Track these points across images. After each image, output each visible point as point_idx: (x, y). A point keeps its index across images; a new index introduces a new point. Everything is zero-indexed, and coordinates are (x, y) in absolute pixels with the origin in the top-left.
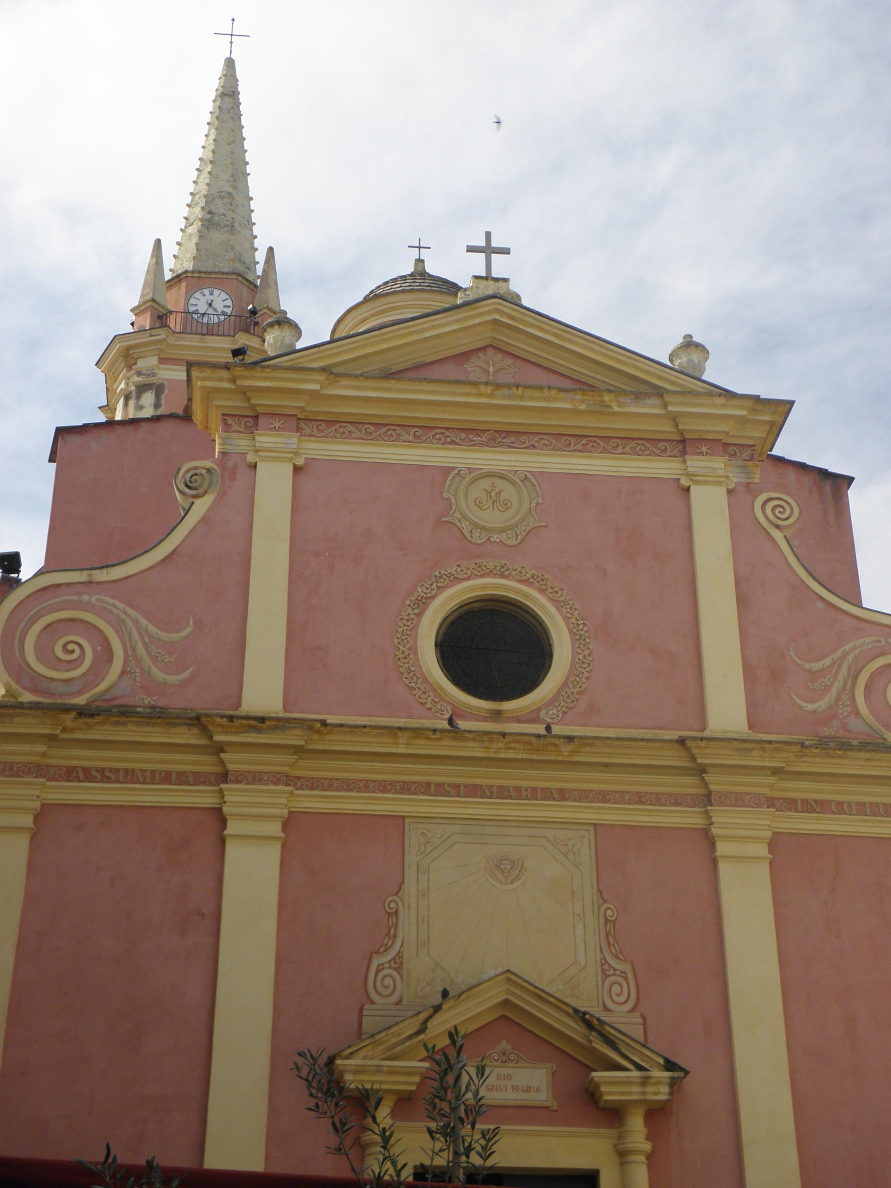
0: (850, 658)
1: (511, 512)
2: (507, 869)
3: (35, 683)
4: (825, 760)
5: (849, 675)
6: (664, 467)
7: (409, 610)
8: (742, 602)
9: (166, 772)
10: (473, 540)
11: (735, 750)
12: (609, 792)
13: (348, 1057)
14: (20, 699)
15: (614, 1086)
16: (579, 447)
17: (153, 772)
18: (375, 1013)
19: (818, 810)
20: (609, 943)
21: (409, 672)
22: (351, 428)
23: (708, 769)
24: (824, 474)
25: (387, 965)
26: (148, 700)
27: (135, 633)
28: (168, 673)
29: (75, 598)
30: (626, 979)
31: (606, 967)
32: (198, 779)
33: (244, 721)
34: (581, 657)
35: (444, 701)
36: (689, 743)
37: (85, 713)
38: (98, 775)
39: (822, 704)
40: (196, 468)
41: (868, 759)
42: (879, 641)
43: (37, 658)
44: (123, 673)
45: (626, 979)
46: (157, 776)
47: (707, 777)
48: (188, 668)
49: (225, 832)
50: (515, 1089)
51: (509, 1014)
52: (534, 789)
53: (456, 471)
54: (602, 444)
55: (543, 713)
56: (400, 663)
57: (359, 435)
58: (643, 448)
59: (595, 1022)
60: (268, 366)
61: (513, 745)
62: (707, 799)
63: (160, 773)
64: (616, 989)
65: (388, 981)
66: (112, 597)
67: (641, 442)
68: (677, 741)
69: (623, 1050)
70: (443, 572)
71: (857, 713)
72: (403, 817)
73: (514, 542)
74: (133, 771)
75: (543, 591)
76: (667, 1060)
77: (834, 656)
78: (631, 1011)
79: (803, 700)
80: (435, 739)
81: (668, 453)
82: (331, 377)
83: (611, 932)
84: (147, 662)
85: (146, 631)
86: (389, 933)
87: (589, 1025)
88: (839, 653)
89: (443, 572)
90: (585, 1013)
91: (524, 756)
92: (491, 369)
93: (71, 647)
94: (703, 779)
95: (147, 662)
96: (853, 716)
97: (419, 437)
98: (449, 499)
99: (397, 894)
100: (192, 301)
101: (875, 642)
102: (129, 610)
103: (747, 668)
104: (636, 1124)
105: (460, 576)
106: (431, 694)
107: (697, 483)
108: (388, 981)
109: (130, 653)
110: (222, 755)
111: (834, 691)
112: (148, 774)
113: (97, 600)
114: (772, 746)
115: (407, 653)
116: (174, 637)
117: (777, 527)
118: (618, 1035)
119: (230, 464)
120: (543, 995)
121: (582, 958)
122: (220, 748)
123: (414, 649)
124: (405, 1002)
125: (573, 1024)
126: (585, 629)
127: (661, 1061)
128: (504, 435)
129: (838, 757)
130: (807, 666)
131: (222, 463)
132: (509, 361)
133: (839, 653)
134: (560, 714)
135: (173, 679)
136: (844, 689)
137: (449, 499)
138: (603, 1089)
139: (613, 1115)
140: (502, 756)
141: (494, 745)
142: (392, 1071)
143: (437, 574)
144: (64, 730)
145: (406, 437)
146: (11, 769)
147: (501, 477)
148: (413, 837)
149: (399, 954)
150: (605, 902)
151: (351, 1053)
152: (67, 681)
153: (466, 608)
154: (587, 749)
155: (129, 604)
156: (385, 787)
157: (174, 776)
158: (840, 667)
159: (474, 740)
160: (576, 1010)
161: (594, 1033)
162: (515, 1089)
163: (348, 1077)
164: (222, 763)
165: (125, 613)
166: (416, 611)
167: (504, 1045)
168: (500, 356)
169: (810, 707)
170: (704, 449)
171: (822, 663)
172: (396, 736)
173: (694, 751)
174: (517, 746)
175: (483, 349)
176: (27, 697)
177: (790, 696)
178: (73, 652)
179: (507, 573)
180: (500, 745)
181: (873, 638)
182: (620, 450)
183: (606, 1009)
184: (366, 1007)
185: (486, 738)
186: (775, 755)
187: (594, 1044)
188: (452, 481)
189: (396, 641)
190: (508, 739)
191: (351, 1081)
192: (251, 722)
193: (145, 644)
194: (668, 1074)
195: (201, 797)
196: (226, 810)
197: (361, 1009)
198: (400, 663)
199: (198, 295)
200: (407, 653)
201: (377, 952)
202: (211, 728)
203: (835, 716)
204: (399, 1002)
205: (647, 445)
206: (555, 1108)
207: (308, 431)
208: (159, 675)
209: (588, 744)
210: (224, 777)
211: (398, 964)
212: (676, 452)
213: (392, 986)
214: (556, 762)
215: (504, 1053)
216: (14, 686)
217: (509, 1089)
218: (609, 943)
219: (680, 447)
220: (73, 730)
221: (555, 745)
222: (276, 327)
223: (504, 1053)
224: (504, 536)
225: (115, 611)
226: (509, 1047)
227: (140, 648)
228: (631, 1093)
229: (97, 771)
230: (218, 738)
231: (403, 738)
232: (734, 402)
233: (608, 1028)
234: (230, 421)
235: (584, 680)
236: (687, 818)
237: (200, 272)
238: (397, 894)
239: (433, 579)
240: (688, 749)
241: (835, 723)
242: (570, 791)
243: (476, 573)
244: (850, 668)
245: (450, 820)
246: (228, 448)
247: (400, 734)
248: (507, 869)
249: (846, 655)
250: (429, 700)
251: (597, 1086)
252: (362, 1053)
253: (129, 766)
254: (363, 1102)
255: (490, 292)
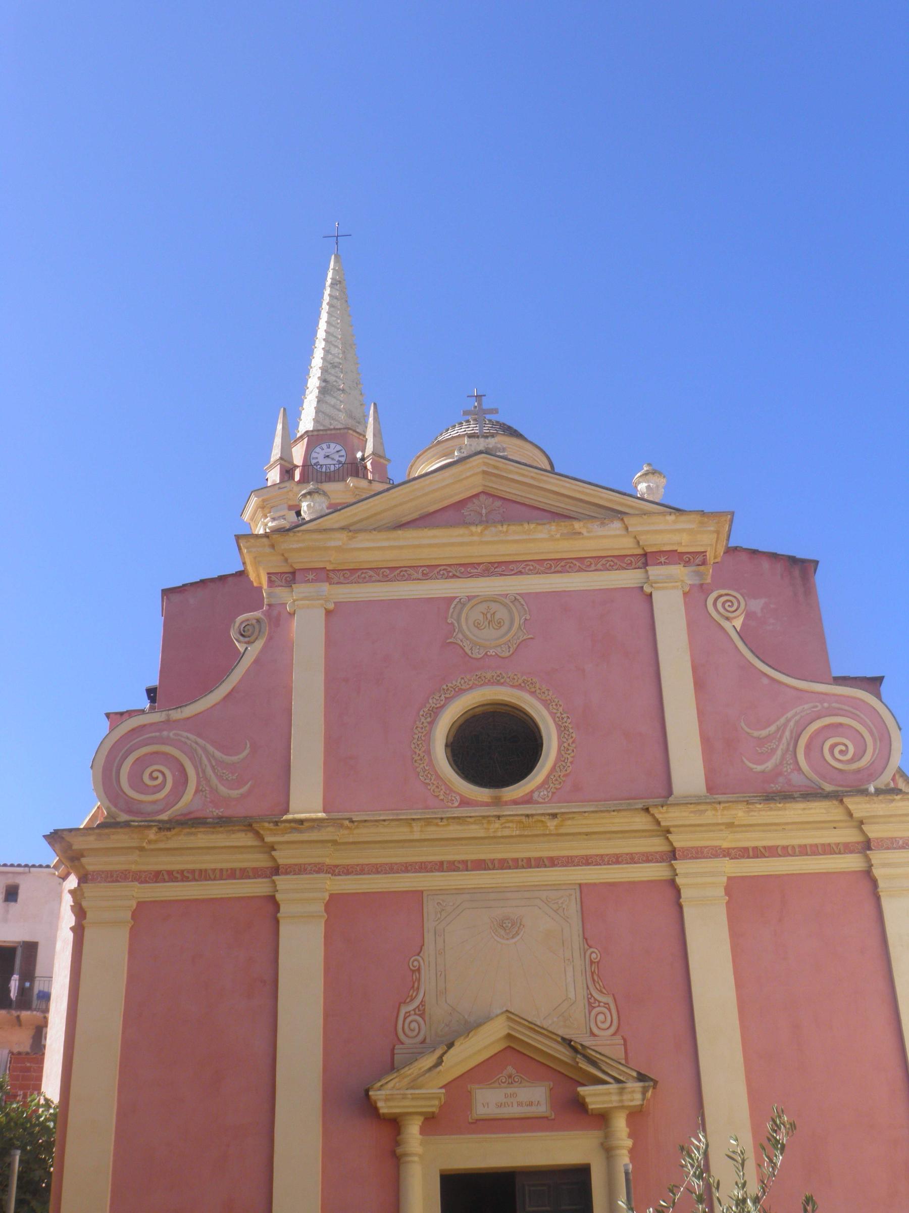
0: (792, 723)
1: (504, 629)
2: (509, 927)
3: (130, 807)
4: (769, 813)
5: (791, 738)
6: (628, 578)
7: (423, 719)
8: (700, 685)
9: (231, 869)
10: (474, 656)
11: (692, 812)
12: (591, 856)
13: (379, 1090)
14: (118, 820)
15: (595, 1097)
16: (559, 568)
17: (221, 870)
18: (405, 1051)
19: (767, 854)
20: (594, 980)
21: (424, 770)
22: (371, 573)
23: (672, 829)
24: (793, 561)
25: (412, 1012)
26: (217, 812)
27: (204, 758)
28: (231, 789)
29: (157, 734)
30: (609, 1010)
31: (592, 1000)
32: (256, 873)
33: (287, 825)
34: (565, 745)
35: (454, 792)
36: (652, 810)
37: (166, 827)
38: (178, 876)
39: (769, 765)
40: (248, 620)
41: (804, 809)
42: (816, 707)
43: (131, 786)
44: (197, 791)
45: (609, 1010)
46: (225, 873)
47: (670, 836)
48: (246, 783)
49: (279, 915)
50: (520, 1104)
51: (512, 1045)
52: (529, 859)
53: (457, 600)
54: (578, 564)
55: (535, 795)
56: (417, 765)
57: (378, 578)
58: (612, 563)
59: (579, 1047)
60: (298, 531)
61: (507, 825)
62: (673, 854)
63: (227, 870)
64: (601, 1017)
65: (414, 1025)
66: (187, 731)
67: (610, 559)
68: (642, 809)
69: (604, 1068)
70: (449, 685)
71: (799, 769)
72: (422, 892)
73: (507, 654)
74: (206, 870)
75: (533, 693)
76: (639, 1073)
77: (778, 723)
78: (614, 1034)
79: (754, 763)
80: (443, 826)
81: (633, 566)
82: (350, 534)
83: (596, 972)
84: (214, 780)
85: (213, 756)
86: (413, 987)
87: (575, 1050)
88: (782, 720)
89: (449, 685)
90: (571, 1041)
91: (518, 833)
92: (484, 511)
93: (155, 774)
94: (667, 838)
95: (214, 780)
96: (796, 772)
97: (426, 574)
98: (452, 623)
99: (418, 954)
100: (314, 455)
101: (814, 707)
102: (199, 740)
103: (706, 741)
104: (620, 1124)
105: (463, 687)
106: (443, 787)
107: (658, 589)
108: (414, 1025)
109: (201, 775)
110: (274, 853)
111: (779, 753)
112: (217, 872)
113: (175, 735)
114: (723, 805)
115: (422, 755)
116: (235, 759)
117: (728, 619)
118: (598, 1056)
119: (275, 613)
120: (536, 1028)
121: (572, 995)
122: (272, 848)
123: (428, 752)
124: (428, 1040)
125: (563, 1050)
126: (569, 721)
127: (635, 1074)
128: (496, 565)
129: (779, 809)
130: (756, 734)
131: (268, 614)
132: (498, 503)
133: (782, 720)
134: (550, 794)
135: (235, 793)
136: (787, 750)
137: (452, 623)
138: (588, 1100)
139: (602, 1119)
140: (499, 834)
141: (492, 826)
142: (415, 1098)
143: (445, 687)
144: (150, 842)
145: (415, 576)
146: (112, 876)
147: (495, 601)
148: (429, 907)
149: (422, 1003)
150: (590, 947)
151: (382, 1086)
152: (154, 802)
153: (471, 712)
154: (569, 822)
155: (199, 735)
156: (407, 868)
157: (238, 872)
158: (783, 732)
159: (474, 823)
160: (563, 1039)
161: (579, 1056)
162: (520, 1104)
163: (380, 1104)
164: (274, 859)
165: (196, 743)
166: (429, 720)
167: (510, 1070)
168: (491, 499)
169: (759, 768)
170: (663, 560)
171: (768, 730)
172: (410, 826)
173: (658, 816)
174: (510, 825)
175: (477, 496)
176: (123, 817)
177: (742, 761)
178: (157, 778)
179: (502, 681)
180: (497, 825)
181: (811, 705)
182: (593, 567)
183: (592, 1034)
184: (397, 1047)
185: (485, 821)
186: (725, 812)
187: (580, 1065)
188: (454, 608)
189: (413, 746)
190: (503, 820)
191: (384, 1108)
192: (293, 825)
193: (213, 767)
194: (641, 1084)
195: (257, 888)
196: (278, 897)
197: (393, 1049)
198: (417, 765)
199: (318, 449)
200: (422, 755)
201: (404, 1003)
202: (262, 832)
203: (780, 774)
204: (423, 1042)
205: (616, 561)
206: (553, 1117)
207: (336, 580)
208: (223, 790)
209: (569, 819)
210: (276, 870)
211: (421, 1011)
212: (640, 564)
213: (417, 1031)
214: (544, 835)
215: (510, 1077)
216: (113, 809)
217: (515, 1105)
218: (594, 980)
219: (643, 560)
220: (156, 841)
221: (542, 821)
222: (308, 497)
223: (510, 1077)
224: (499, 649)
225: (189, 742)
226: (514, 1071)
227: (209, 770)
228: (611, 1101)
229: (188, 872)
230: (269, 839)
231: (416, 827)
232: (684, 518)
233: (590, 1052)
234: (273, 578)
235: (568, 764)
236: (655, 872)
237: (319, 430)
238: (418, 954)
239: (442, 692)
240: (653, 815)
241: (781, 780)
242: (558, 858)
243: (476, 682)
244: (792, 732)
245: (460, 891)
246: (273, 601)
247: (414, 824)
248: (509, 927)
249: (788, 721)
250: (442, 793)
251: (584, 1098)
252: (391, 1085)
253: (204, 866)
254: (395, 1124)
255: (481, 447)
